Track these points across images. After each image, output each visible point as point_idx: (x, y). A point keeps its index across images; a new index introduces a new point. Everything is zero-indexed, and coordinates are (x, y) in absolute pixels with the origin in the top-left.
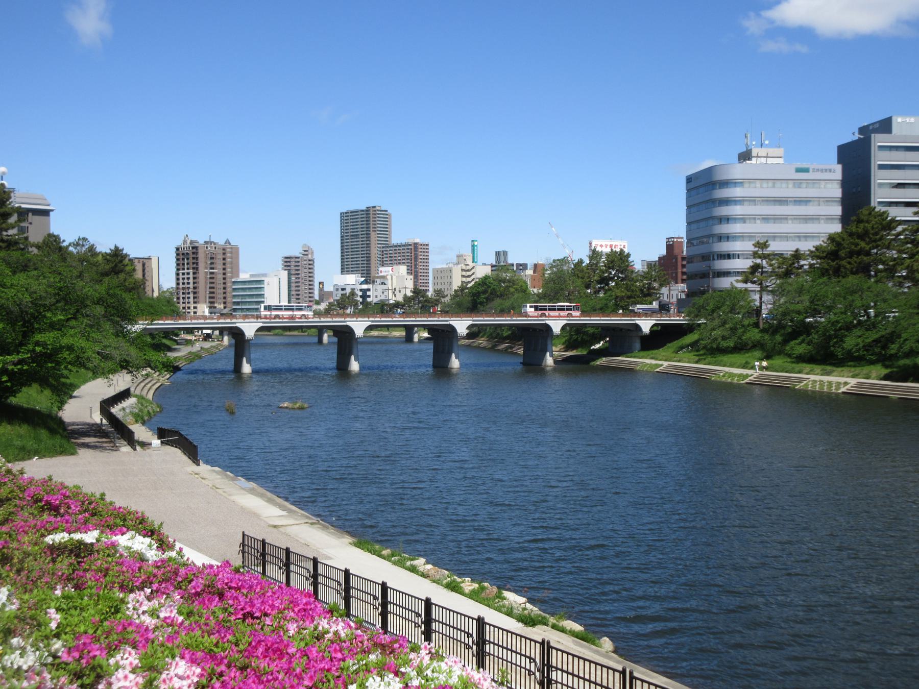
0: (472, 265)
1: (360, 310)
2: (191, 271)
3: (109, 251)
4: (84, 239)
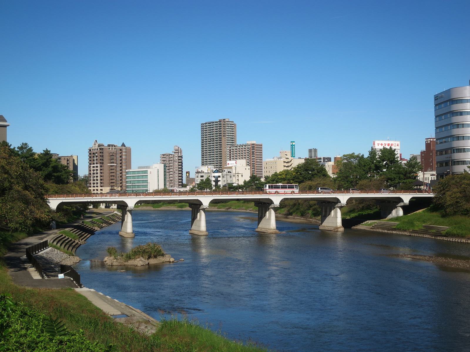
0: (290, 158)
1: (214, 190)
2: (98, 165)
3: (42, 152)
4: (26, 144)
